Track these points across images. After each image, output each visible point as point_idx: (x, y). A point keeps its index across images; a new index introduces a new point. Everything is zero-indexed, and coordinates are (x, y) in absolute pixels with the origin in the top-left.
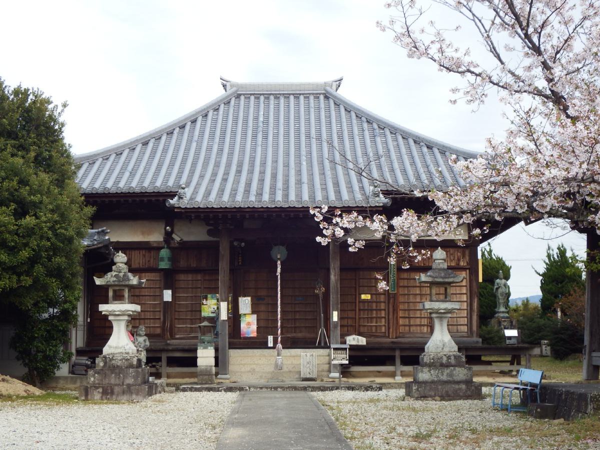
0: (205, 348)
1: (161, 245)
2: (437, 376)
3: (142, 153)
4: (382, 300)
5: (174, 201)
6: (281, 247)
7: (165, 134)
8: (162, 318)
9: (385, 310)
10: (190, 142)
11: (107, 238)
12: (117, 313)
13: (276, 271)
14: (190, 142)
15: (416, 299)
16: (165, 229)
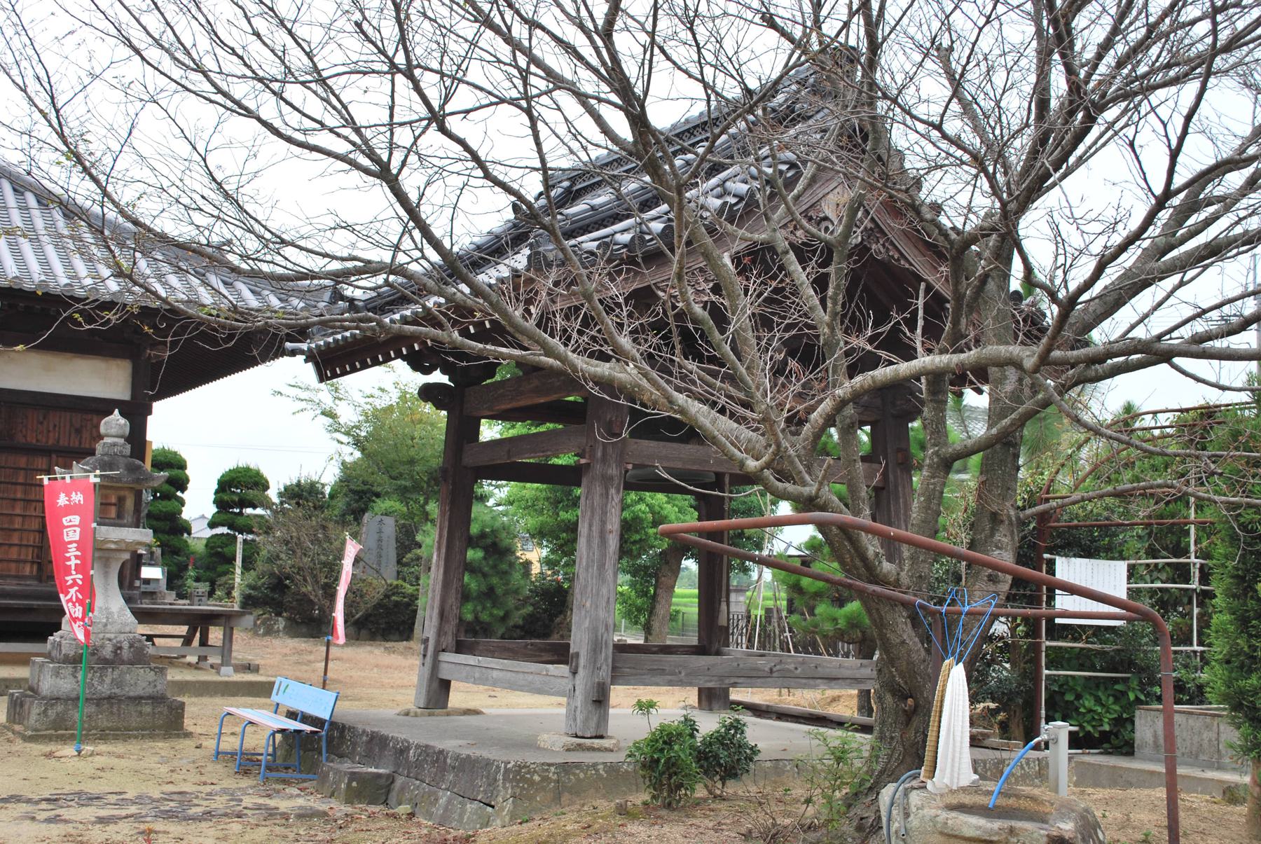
15: (13, 508)
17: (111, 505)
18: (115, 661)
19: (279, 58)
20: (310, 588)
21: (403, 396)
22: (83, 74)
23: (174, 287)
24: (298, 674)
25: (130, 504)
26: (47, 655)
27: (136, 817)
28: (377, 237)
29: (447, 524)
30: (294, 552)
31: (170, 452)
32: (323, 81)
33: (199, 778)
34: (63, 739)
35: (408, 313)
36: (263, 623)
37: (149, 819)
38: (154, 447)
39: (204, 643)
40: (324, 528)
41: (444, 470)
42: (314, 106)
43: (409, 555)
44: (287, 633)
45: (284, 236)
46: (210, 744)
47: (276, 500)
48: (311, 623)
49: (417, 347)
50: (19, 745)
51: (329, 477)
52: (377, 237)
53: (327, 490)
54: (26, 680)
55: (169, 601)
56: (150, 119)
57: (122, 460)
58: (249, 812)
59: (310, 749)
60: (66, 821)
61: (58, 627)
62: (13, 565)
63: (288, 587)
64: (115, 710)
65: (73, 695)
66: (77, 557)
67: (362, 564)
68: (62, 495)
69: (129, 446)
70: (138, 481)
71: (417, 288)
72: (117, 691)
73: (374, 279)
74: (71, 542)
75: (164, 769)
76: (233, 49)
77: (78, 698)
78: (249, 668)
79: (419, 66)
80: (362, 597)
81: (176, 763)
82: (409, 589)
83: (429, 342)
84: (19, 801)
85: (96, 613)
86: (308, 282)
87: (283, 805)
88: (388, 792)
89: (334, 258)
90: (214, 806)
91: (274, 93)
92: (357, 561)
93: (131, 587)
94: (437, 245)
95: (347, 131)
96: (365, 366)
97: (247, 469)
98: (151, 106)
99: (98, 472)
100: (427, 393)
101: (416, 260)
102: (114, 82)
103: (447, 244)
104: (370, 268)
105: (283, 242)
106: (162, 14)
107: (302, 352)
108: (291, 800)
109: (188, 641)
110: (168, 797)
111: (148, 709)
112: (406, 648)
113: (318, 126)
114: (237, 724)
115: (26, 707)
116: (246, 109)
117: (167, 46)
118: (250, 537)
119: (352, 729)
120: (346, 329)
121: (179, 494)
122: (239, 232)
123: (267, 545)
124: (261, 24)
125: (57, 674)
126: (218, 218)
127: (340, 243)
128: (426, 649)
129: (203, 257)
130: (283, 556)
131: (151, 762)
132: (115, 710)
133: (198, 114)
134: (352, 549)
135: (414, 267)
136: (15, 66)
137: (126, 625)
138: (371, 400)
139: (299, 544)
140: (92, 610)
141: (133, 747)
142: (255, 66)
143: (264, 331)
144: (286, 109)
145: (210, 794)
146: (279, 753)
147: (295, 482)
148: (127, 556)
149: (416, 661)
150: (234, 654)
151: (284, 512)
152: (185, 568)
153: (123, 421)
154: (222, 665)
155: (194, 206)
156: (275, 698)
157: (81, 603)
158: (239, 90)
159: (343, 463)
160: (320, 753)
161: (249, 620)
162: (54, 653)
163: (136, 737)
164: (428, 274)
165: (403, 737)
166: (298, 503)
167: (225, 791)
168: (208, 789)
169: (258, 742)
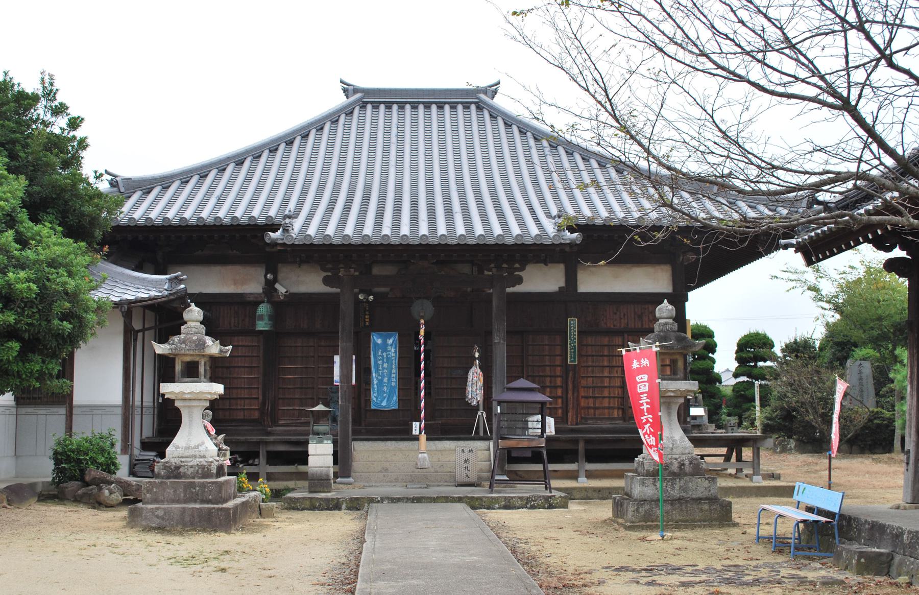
0: (321, 442)
1: (259, 299)
2: (665, 491)
3: (234, 177)
4: (558, 374)
5: (276, 235)
6: (425, 301)
7: (267, 151)
8: (261, 398)
9: (561, 387)
10: (299, 161)
11: (182, 286)
12: (187, 396)
13: (418, 334)
14: (299, 161)
15: (603, 372)
16: (265, 276)
17: (668, 366)
18: (676, 476)
19: (760, 36)
20: (811, 417)
21: (868, 270)
22: (624, 71)
23: (706, 210)
24: (809, 479)
25: (680, 364)
26: (635, 471)
27: (706, 582)
28: (844, 154)
29: (916, 363)
30: (797, 391)
31: (701, 326)
32: (793, 47)
33: (746, 555)
34: (652, 528)
35: (870, 207)
36: (780, 444)
37: (715, 584)
38: (691, 324)
39: (739, 459)
40: (818, 372)
41: (909, 323)
42: (789, 66)
43: (884, 389)
44: (797, 451)
45: (776, 163)
46: (753, 531)
47: (780, 354)
48: (814, 442)
49: (879, 232)
50: (622, 533)
51: (817, 333)
52: (844, 154)
53: (817, 344)
54: (623, 489)
55: (711, 430)
56: (675, 98)
57: (672, 334)
58: (786, 580)
59: (826, 534)
60: (660, 585)
61: (641, 452)
62: (606, 411)
63: (795, 417)
64: (684, 508)
65: (655, 497)
66: (647, 403)
67: (848, 397)
68: (635, 361)
69: (676, 324)
70: (684, 348)
71: (875, 187)
72: (684, 494)
73: (844, 185)
74: (643, 393)
75: (722, 549)
76: (726, 35)
77: (658, 500)
78: (772, 476)
79: (867, 21)
80: (851, 421)
81: (729, 545)
82: (887, 414)
83: (889, 227)
84: (627, 570)
85: (665, 441)
86: (795, 194)
87: (811, 575)
88: (889, 567)
89: (815, 174)
90: (760, 575)
91: (759, 61)
92: (846, 395)
93: (685, 422)
94: (891, 153)
95: (815, 80)
96: (840, 251)
97: (757, 334)
98: (673, 85)
99: (657, 344)
100: (891, 266)
101: (876, 167)
102: (647, 74)
103: (900, 151)
104: (840, 178)
105: (773, 167)
106: (674, 21)
107: (792, 246)
108: (816, 572)
109: (727, 458)
110: (727, 569)
111: (706, 507)
112: (888, 458)
113: (792, 79)
114: (769, 517)
115: (625, 506)
116: (739, 76)
117: (679, 42)
118: (763, 382)
119: (856, 519)
120: (825, 224)
121: (710, 355)
122: (742, 165)
123: (777, 386)
124: (743, 14)
125: (643, 484)
126: (728, 157)
127: (816, 163)
128: (908, 458)
129: (714, 186)
130: (789, 395)
131: (712, 544)
132: (684, 508)
133: (704, 85)
134: (841, 387)
135: (874, 172)
136: (580, 75)
137: (685, 448)
138: (843, 276)
139: (800, 385)
140: (662, 439)
141: (699, 533)
142: (743, 44)
143: (767, 233)
144: (769, 71)
145: (756, 567)
146: (802, 538)
147: (792, 340)
148: (682, 401)
149: (902, 468)
150: (761, 467)
151: (787, 362)
152: (720, 407)
153: (670, 307)
154: (754, 474)
155: (707, 151)
156: (796, 497)
157: (654, 434)
158: (733, 63)
159: (827, 324)
160: (834, 538)
161: (770, 442)
162: (640, 469)
163: (700, 526)
164: (885, 176)
165: (897, 525)
166: (797, 356)
167: (766, 565)
168: (754, 563)
169: (787, 529)
